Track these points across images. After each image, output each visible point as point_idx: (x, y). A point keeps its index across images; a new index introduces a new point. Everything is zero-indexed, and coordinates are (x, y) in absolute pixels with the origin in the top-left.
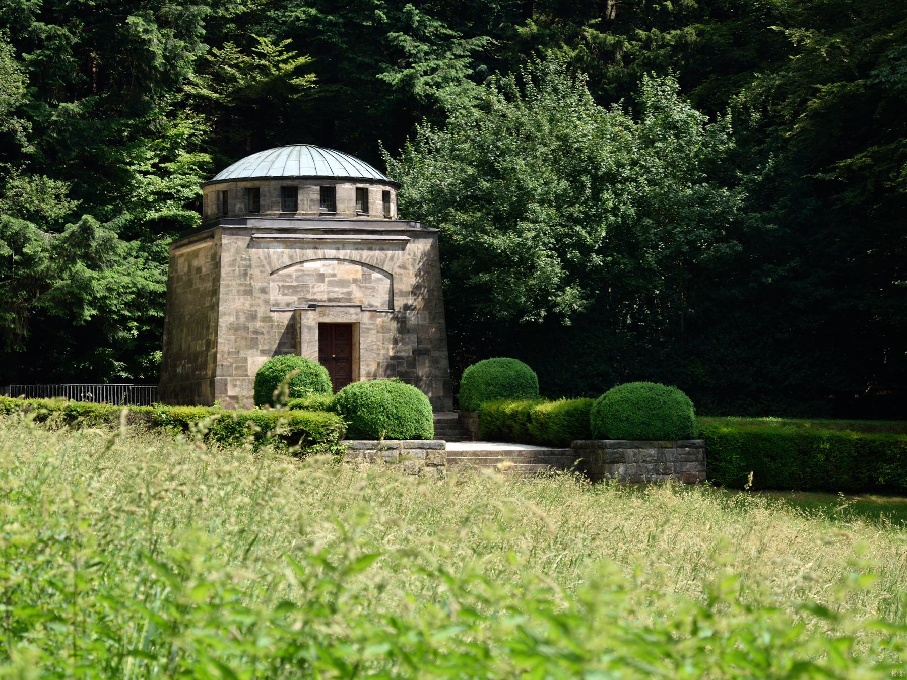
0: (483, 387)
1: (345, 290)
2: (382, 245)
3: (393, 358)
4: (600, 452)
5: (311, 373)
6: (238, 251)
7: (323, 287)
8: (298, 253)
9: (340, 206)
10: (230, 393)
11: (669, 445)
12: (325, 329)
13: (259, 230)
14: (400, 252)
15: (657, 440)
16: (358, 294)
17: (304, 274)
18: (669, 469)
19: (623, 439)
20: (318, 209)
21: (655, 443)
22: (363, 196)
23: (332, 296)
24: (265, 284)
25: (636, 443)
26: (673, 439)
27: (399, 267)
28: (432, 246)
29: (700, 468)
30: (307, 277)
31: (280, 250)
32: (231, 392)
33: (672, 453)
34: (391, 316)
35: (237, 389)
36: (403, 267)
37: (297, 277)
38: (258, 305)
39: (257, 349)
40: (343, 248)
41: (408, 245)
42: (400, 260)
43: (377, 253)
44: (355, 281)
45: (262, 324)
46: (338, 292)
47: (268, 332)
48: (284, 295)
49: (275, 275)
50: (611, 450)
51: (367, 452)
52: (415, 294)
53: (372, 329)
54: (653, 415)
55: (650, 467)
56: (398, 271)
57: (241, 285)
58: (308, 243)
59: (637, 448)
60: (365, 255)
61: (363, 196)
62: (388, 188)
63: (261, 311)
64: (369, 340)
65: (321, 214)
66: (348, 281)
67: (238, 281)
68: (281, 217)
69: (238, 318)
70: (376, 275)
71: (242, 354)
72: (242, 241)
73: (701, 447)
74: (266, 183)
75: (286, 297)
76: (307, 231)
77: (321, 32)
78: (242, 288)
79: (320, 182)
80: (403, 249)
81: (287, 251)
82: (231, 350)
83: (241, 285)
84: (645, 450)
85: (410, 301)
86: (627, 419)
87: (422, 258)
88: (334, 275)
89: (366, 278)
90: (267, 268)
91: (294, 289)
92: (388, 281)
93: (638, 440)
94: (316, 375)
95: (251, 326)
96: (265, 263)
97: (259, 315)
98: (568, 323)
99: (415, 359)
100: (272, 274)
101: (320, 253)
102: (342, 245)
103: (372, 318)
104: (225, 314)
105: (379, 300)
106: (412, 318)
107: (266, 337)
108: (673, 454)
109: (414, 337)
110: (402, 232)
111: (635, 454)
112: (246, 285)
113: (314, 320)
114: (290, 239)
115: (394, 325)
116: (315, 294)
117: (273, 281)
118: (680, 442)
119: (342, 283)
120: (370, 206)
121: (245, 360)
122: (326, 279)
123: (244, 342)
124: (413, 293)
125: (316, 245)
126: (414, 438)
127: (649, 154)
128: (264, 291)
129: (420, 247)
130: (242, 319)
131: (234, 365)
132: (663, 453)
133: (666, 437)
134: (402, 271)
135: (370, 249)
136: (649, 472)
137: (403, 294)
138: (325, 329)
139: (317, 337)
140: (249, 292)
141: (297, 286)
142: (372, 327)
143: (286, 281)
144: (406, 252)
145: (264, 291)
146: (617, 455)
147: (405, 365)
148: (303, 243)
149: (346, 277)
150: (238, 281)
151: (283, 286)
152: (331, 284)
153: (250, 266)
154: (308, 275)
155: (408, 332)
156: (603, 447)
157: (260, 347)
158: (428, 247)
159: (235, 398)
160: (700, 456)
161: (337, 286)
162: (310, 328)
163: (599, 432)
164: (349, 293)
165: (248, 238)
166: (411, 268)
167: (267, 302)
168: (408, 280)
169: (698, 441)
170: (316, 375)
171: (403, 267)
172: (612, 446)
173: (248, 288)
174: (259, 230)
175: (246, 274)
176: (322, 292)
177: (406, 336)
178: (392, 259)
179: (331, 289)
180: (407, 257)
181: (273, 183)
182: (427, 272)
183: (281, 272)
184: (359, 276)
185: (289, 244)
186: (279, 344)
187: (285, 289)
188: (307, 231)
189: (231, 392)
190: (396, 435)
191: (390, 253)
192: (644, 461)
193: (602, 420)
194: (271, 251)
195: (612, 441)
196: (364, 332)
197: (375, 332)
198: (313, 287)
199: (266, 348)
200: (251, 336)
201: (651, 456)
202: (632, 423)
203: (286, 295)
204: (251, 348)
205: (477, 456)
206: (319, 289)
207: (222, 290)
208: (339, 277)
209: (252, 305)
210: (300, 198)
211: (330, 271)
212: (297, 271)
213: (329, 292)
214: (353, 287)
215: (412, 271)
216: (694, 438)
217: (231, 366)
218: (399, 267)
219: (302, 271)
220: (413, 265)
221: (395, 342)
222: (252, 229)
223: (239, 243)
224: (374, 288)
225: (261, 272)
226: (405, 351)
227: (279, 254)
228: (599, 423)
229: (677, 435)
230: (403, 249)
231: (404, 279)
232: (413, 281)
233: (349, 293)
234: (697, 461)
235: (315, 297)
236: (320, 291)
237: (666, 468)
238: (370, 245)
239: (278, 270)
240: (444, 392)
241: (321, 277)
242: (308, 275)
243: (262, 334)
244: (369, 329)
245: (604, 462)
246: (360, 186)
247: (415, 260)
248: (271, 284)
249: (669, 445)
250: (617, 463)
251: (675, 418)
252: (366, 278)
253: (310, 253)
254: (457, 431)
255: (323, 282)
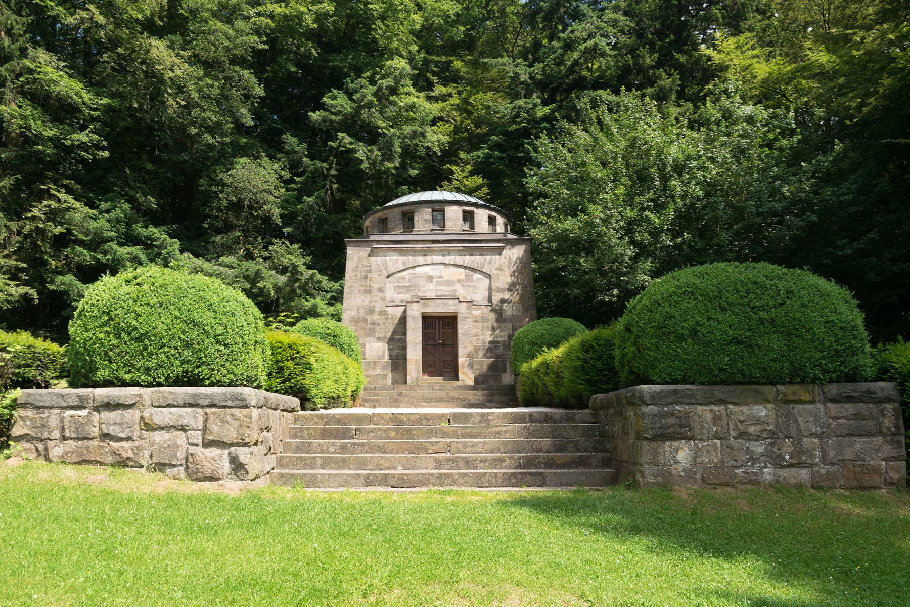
0: (527, 348)
1: (451, 289)
2: (482, 252)
3: (490, 342)
4: (630, 413)
5: (328, 335)
6: (360, 260)
7: (432, 286)
8: (410, 260)
9: (448, 224)
11: (806, 396)
12: (428, 320)
13: (378, 242)
14: (498, 257)
15: (773, 384)
16: (461, 292)
17: (415, 276)
18: (809, 453)
19: (684, 382)
20: (430, 226)
21: (769, 390)
22: (468, 217)
23: (440, 293)
24: (382, 285)
25: (720, 391)
26: (815, 380)
27: (497, 269)
28: (525, 252)
29: (888, 450)
31: (395, 258)
33: (880, 394)
34: (490, 308)
36: (500, 269)
37: (410, 279)
38: (376, 302)
40: (449, 255)
41: (504, 252)
43: (478, 258)
44: (459, 281)
45: (379, 317)
46: (445, 291)
47: (384, 323)
48: (399, 293)
49: (391, 278)
50: (655, 409)
51: (69, 413)
52: (511, 291)
54: (762, 321)
55: (758, 448)
56: (496, 272)
57: (362, 286)
58: (419, 251)
59: (721, 402)
60: (468, 260)
61: (468, 217)
62: (493, 214)
63: (378, 307)
64: (466, 327)
65: (433, 230)
66: (454, 281)
67: (360, 283)
68: (402, 234)
69: (358, 312)
70: (477, 276)
72: (364, 251)
73: (888, 400)
74: (391, 211)
75: (400, 295)
76: (418, 241)
77: (493, 164)
78: (363, 288)
79: (431, 205)
80: (500, 255)
81: (401, 258)
84: (745, 409)
85: (507, 296)
86: (694, 333)
87: (516, 262)
88: (441, 277)
89: (468, 278)
91: (407, 289)
92: (488, 280)
93: (723, 382)
94: (334, 336)
95: (370, 318)
96: (382, 268)
100: (388, 277)
101: (429, 259)
102: (449, 252)
103: (468, 308)
104: (348, 309)
105: (480, 296)
106: (508, 310)
108: (816, 417)
109: (509, 325)
110: (499, 241)
111: (717, 419)
114: (400, 247)
115: (492, 316)
117: (390, 282)
118: (833, 389)
119: (448, 283)
120: (476, 224)
122: (434, 280)
123: (363, 332)
124: (509, 290)
125: (425, 253)
126: (178, 382)
127: (715, 147)
128: (381, 290)
129: (516, 253)
130: (362, 313)
132: (788, 415)
133: (798, 376)
134: (498, 272)
135: (472, 255)
136: (754, 461)
137: (499, 290)
138: (428, 320)
139: (420, 325)
140: (368, 291)
144: (502, 257)
145: (381, 290)
146: (672, 421)
148: (415, 252)
149: (451, 278)
150: (360, 283)
152: (438, 283)
153: (370, 271)
154: (419, 277)
155: (504, 321)
156: (637, 401)
157: (377, 335)
158: (521, 253)
160: (888, 422)
162: (414, 318)
163: (632, 373)
164: (454, 291)
165: (369, 249)
166: (506, 269)
167: (383, 299)
168: (504, 279)
169: (884, 387)
170: (334, 336)
171: (500, 269)
172: (656, 399)
174: (378, 242)
175: (366, 277)
176: (431, 290)
177: (503, 325)
178: (490, 262)
179: (439, 288)
180: (503, 260)
181: (396, 210)
182: (520, 273)
183: (396, 275)
184: (463, 277)
185: (401, 252)
186: (393, 333)
187: (400, 289)
188: (418, 241)
190: (135, 375)
191: (488, 258)
192: (742, 435)
193: (635, 344)
194: (388, 258)
195: (656, 388)
197: (471, 320)
199: (382, 335)
200: (369, 326)
201: (758, 421)
202: (709, 343)
204: (369, 336)
205: (401, 422)
208: (445, 278)
209: (370, 302)
210: (416, 219)
211: (438, 274)
213: (436, 291)
214: (458, 286)
215: (507, 272)
216: (866, 380)
218: (497, 269)
220: (508, 267)
221: (494, 329)
222: (372, 241)
223: (362, 253)
226: (501, 336)
227: (394, 261)
228: (630, 350)
229: (825, 371)
230: (500, 255)
231: (501, 278)
232: (509, 280)
233: (454, 291)
234: (880, 433)
236: (429, 290)
237: (799, 451)
238: (471, 252)
241: (430, 279)
242: (419, 277)
243: (379, 324)
245: (639, 437)
247: (510, 263)
248: (388, 285)
249: (806, 396)
250: (672, 438)
251: (820, 330)
252: (468, 278)
253: (420, 260)
254: (505, 398)
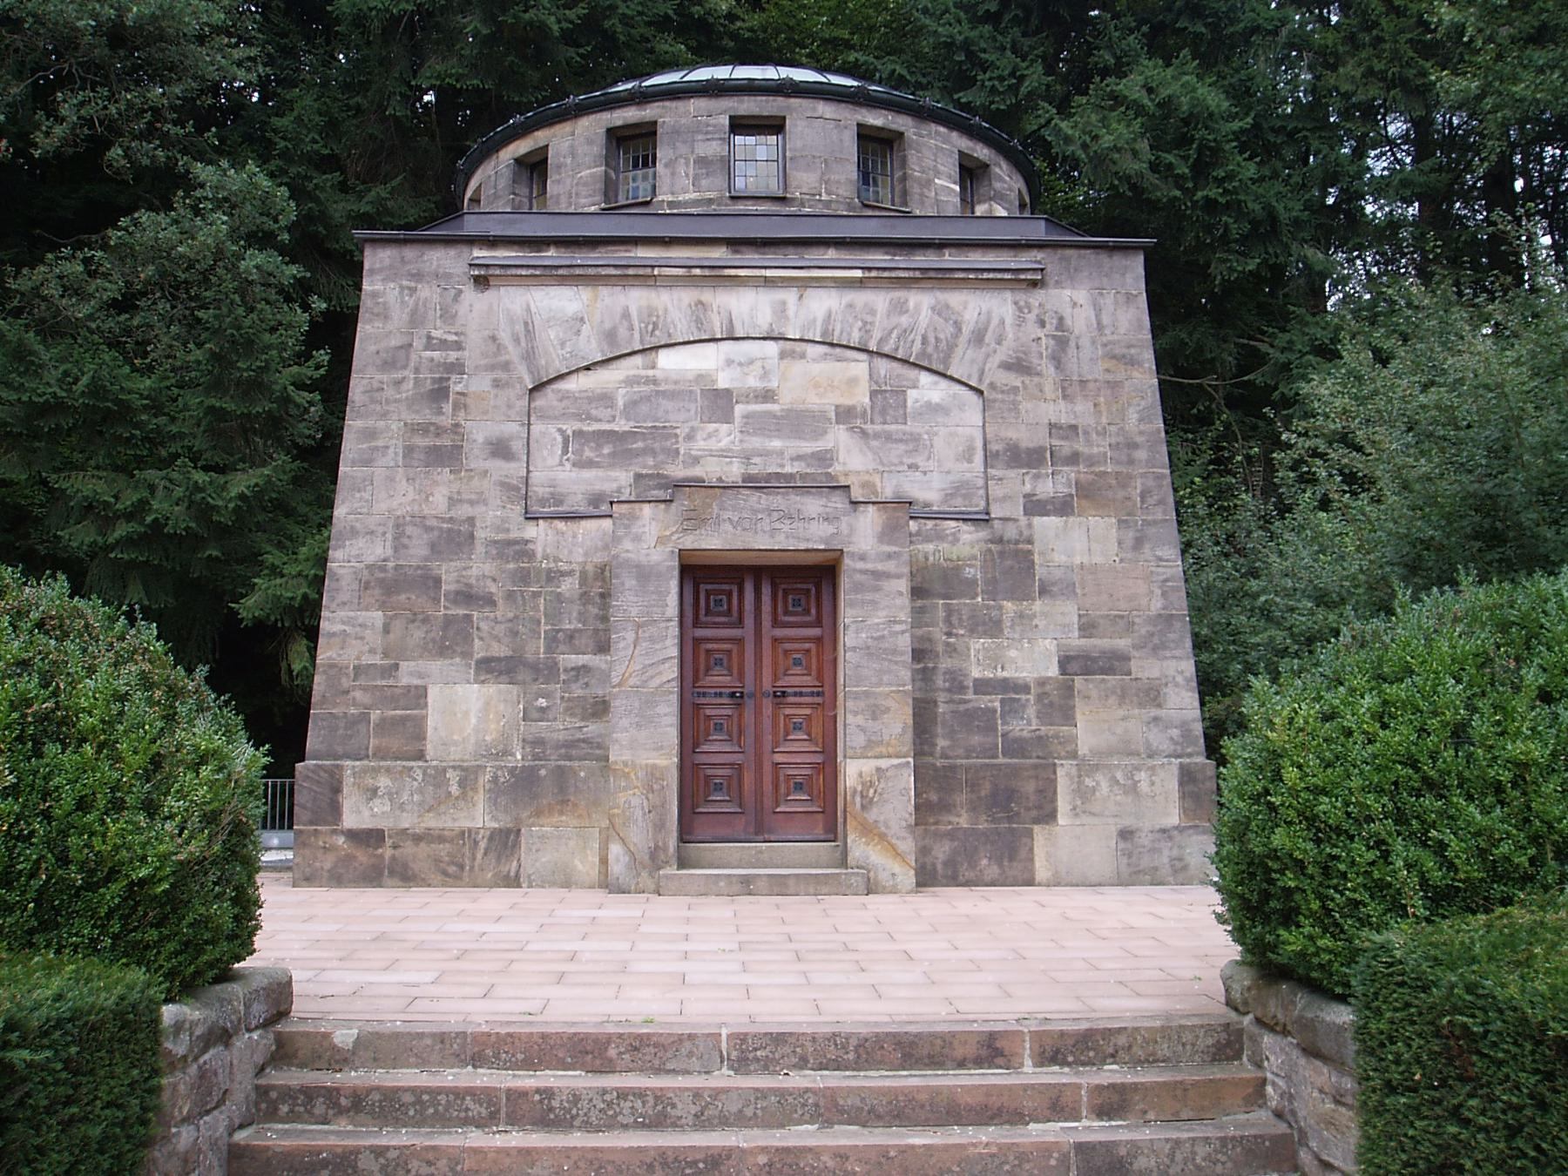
1: (808, 447)
7: (725, 436)
10: (350, 821)
16: (853, 459)
17: (658, 392)
23: (758, 467)
27: (1006, 366)
30: (666, 404)
32: (355, 814)
35: (380, 806)
37: (632, 405)
39: (467, 655)
42: (1010, 341)
44: (845, 415)
46: (783, 453)
47: (510, 596)
48: (581, 464)
53: (887, 575)
64: (879, 618)
69: (399, 546)
71: (406, 676)
75: (588, 474)
82: (367, 660)
83: (423, 429)
88: (768, 396)
90: (522, 370)
91: (620, 445)
96: (513, 353)
97: (480, 534)
98: (1368, 296)
99: (1068, 689)
103: (889, 533)
104: (354, 533)
107: (503, 611)
112: (440, 431)
113: (661, 540)
116: (696, 460)
119: (799, 422)
121: (418, 696)
122: (739, 409)
130: (418, 550)
131: (375, 715)
134: (1014, 380)
141: (631, 435)
142: (890, 566)
143: (589, 417)
147: (1031, 711)
149: (814, 401)
151: (578, 434)
152: (755, 424)
153: (458, 368)
155: (1044, 591)
159: (370, 838)
161: (778, 432)
162: (644, 574)
164: (824, 458)
173: (446, 441)
175: (439, 393)
176: (723, 454)
179: (756, 442)
187: (589, 444)
189: (355, 814)
196: (858, 588)
197: (903, 585)
198: (690, 437)
203: (590, 464)
206: (713, 444)
207: (350, 447)
208: (788, 397)
209: (453, 502)
212: (630, 382)
213: (747, 458)
214: (838, 437)
217: (365, 718)
218: (1006, 366)
219: (655, 381)
224: (915, 439)
225: (497, 384)
231: (1025, 406)
235: (697, 472)
239: (550, 381)
240: (1185, 811)
241: (719, 403)
243: (490, 601)
244: (878, 575)
246: (876, 119)
255: (727, 418)
